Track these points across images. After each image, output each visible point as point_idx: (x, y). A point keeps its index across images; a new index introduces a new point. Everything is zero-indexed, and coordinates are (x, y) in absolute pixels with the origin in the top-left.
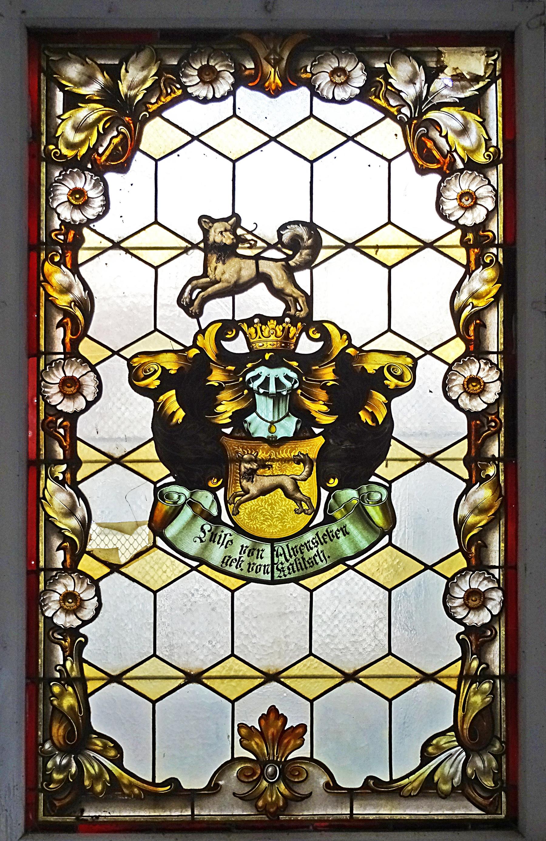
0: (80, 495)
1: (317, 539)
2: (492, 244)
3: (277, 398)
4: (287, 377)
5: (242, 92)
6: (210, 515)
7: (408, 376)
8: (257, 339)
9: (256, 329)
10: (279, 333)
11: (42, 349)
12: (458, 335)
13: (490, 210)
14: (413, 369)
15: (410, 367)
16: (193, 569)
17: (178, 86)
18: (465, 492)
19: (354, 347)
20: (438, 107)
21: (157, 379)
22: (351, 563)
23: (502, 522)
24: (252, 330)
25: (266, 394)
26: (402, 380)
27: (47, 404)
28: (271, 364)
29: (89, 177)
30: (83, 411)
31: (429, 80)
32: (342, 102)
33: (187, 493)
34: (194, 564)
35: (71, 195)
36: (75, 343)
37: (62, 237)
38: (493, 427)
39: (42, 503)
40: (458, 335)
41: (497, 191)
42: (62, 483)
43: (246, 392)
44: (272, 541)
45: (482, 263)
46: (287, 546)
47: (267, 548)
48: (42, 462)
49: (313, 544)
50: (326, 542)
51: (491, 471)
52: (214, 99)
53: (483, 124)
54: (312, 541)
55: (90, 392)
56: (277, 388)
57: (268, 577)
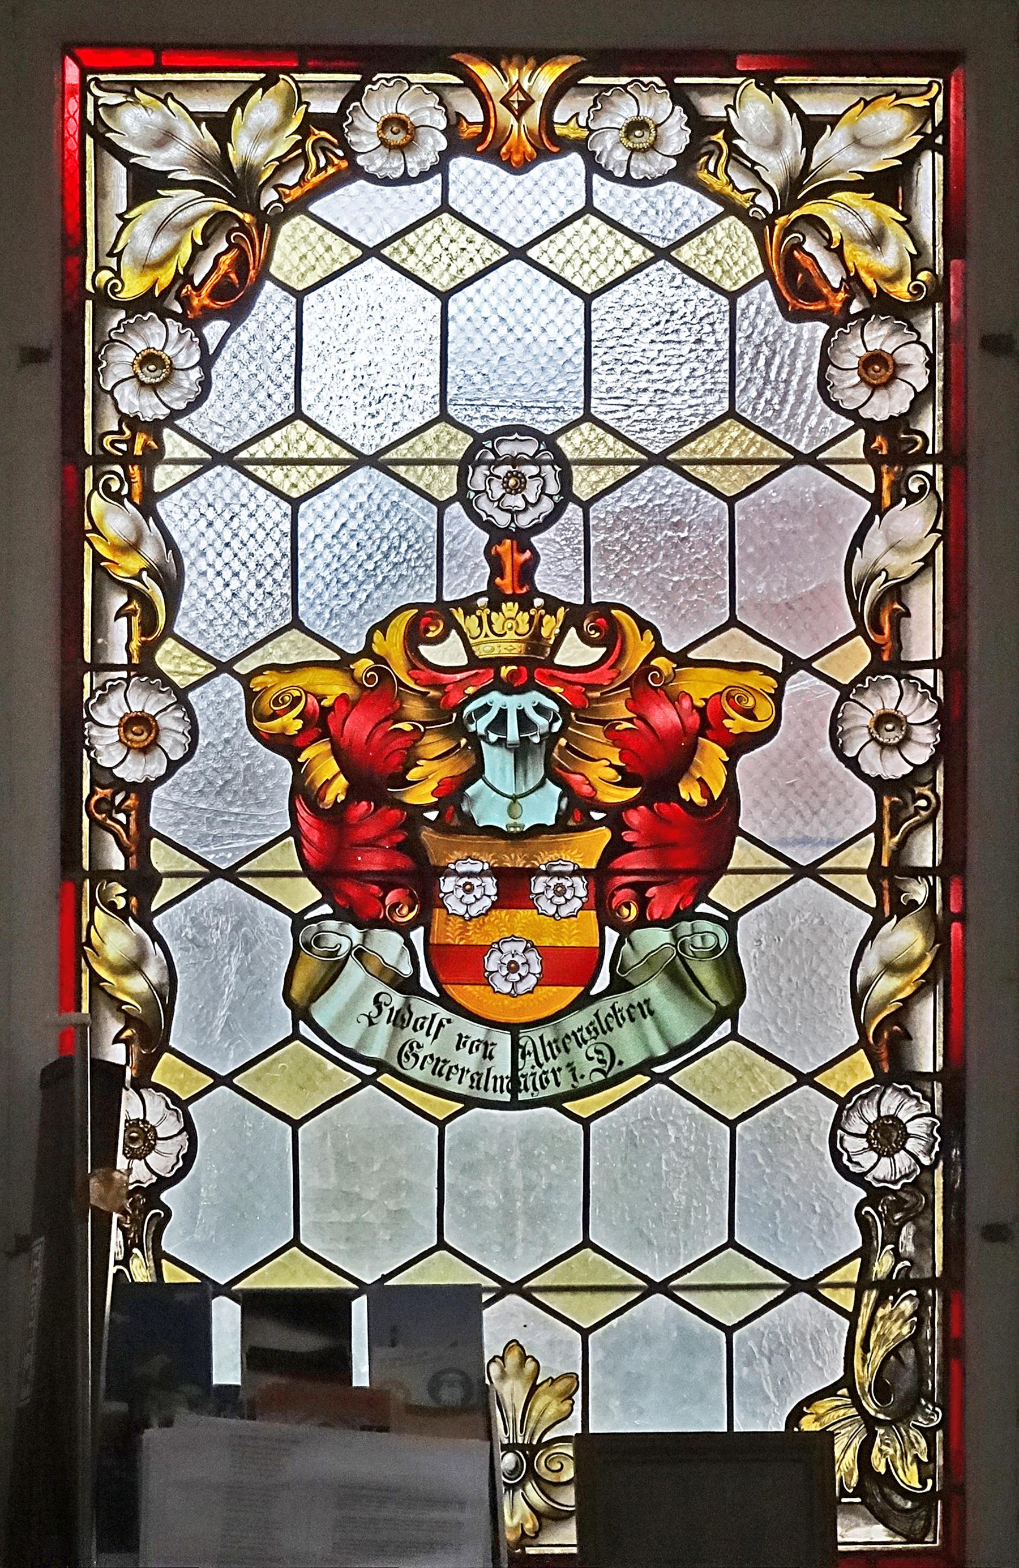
0: (156, 938)
1: (597, 1025)
2: (922, 457)
3: (521, 752)
4: (540, 709)
5: (461, 166)
6: (397, 975)
7: (765, 710)
8: (482, 638)
9: (480, 618)
10: (524, 628)
11: (88, 658)
12: (860, 631)
13: (919, 390)
14: (777, 697)
15: (769, 695)
16: (366, 1081)
17: (340, 153)
18: (871, 934)
19: (668, 655)
20: (823, 192)
21: (297, 718)
22: (659, 1069)
23: (939, 988)
24: (473, 620)
25: (501, 742)
26: (754, 718)
27: (93, 762)
28: (508, 688)
29: (174, 334)
30: (161, 780)
31: (809, 142)
32: (645, 183)
33: (355, 934)
34: (369, 1071)
35: (142, 365)
36: (148, 650)
37: (123, 447)
38: (925, 809)
39: (84, 953)
40: (860, 631)
41: (932, 357)
42: (124, 914)
43: (463, 741)
44: (514, 1029)
45: (905, 493)
46: (541, 1038)
47: (503, 1041)
48: (86, 875)
49: (589, 1032)
50: (611, 1029)
51: (919, 892)
52: (405, 179)
53: (908, 225)
54: (587, 1029)
55: (173, 744)
56: (520, 731)
57: (507, 1097)
